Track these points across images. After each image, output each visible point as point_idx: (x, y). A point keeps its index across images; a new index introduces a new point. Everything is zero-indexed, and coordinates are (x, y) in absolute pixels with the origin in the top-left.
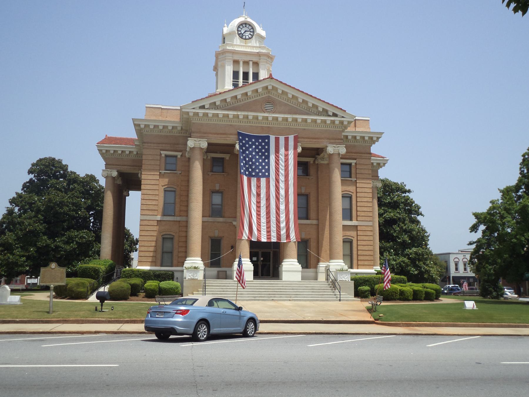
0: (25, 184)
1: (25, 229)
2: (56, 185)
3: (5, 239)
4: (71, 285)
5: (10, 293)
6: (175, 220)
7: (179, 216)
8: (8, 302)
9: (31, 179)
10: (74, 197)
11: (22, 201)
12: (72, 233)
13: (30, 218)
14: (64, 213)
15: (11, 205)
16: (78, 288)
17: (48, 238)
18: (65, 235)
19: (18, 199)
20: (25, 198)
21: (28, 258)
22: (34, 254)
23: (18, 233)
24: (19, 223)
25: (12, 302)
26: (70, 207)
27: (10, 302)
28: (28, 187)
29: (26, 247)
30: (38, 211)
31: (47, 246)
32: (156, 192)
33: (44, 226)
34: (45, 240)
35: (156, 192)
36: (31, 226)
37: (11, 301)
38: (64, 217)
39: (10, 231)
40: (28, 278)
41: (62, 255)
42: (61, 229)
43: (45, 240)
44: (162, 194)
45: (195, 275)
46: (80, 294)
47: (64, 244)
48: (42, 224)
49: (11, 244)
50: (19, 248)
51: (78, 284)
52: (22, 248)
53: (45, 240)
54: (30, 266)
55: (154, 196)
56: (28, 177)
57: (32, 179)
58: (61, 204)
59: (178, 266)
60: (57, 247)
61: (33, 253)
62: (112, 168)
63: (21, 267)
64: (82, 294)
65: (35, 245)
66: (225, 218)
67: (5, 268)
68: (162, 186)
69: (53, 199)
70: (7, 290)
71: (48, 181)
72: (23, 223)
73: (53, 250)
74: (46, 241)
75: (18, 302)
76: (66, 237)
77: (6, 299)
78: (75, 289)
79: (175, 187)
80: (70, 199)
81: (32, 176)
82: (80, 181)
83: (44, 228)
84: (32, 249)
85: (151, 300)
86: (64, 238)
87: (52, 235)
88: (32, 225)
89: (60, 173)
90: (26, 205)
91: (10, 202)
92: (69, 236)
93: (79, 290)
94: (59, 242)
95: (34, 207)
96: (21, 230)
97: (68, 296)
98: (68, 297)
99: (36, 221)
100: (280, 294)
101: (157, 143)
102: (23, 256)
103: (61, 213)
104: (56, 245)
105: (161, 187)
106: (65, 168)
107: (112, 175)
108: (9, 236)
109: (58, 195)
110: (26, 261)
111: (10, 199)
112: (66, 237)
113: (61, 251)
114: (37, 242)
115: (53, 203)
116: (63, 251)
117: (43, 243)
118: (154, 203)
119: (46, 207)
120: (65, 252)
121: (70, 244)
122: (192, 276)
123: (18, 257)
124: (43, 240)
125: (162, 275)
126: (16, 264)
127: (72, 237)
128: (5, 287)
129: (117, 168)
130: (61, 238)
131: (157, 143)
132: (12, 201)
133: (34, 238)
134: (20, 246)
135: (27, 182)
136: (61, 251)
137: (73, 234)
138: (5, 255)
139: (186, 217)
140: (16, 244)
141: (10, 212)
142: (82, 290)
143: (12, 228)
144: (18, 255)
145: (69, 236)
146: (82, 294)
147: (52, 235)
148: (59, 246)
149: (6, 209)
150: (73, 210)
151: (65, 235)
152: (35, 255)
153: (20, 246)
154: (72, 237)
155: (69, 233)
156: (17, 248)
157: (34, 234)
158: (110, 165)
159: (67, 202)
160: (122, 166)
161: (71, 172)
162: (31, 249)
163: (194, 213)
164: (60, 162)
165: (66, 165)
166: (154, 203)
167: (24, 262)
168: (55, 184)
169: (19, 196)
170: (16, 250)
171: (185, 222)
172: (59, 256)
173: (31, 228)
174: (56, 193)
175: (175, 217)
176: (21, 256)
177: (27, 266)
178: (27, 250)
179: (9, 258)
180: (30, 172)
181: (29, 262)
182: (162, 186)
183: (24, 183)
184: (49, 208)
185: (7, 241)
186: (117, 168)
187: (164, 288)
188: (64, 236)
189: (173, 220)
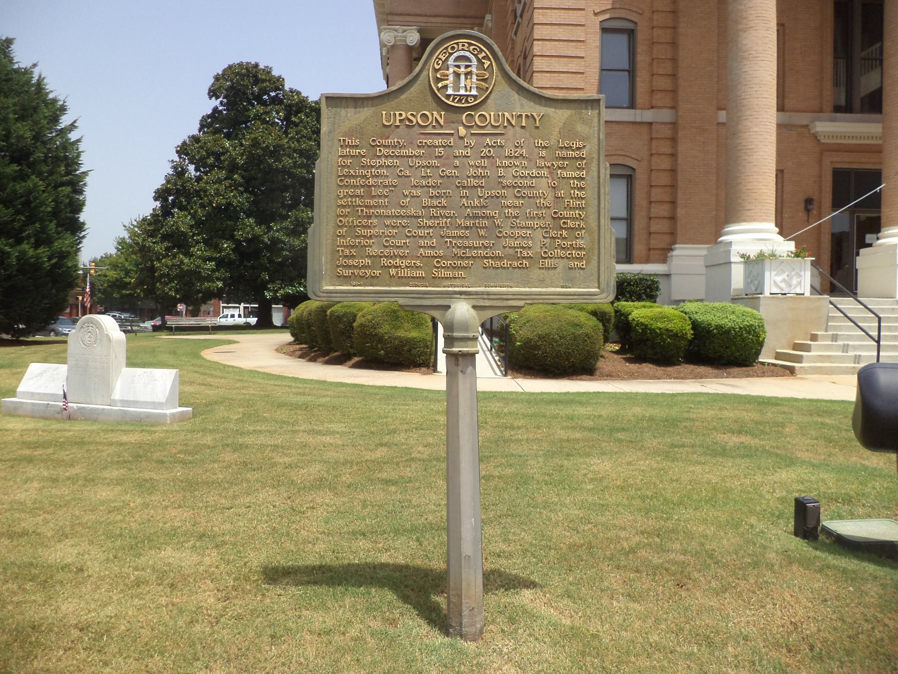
0: (204, 119)
1: (211, 203)
2: (263, 116)
3: (173, 225)
4: (369, 317)
5: (122, 357)
6: (638, 120)
7: (649, 109)
8: (113, 403)
9: (215, 110)
10: (301, 138)
11: (201, 147)
12: (303, 212)
13: (219, 181)
14: (285, 171)
15: (180, 158)
16: (397, 328)
17: (255, 222)
18: (289, 217)
19: (193, 145)
20: (205, 143)
21: (220, 263)
22: (230, 254)
23: (196, 212)
24: (197, 193)
25: (135, 403)
26: (296, 158)
27: (125, 403)
28: (209, 125)
29: (215, 240)
30: (233, 168)
31: (256, 239)
32: (579, 33)
33: (247, 198)
34: (251, 226)
35: (579, 33)
36: (221, 195)
37: (131, 398)
38: (284, 179)
39: (181, 208)
40: (224, 307)
41: (286, 258)
42: (280, 205)
43: (249, 227)
44: (594, 39)
45: (794, 282)
46: (410, 351)
47: (288, 235)
48: (242, 193)
49: (184, 234)
50: (200, 243)
51: (395, 312)
52: (206, 242)
53: (249, 227)
54: (224, 280)
55: (575, 44)
56: (209, 105)
57: (217, 108)
58: (276, 152)
59: (647, 261)
60: (275, 241)
61: (228, 254)
62: (406, 24)
63: (208, 281)
64: (414, 351)
65: (232, 237)
66: (788, 114)
67: (177, 284)
68: (596, 14)
69: (261, 140)
70: (109, 340)
71: (248, 110)
72: (205, 191)
73: (268, 248)
74: (253, 229)
75: (168, 402)
76: (290, 222)
77: (108, 387)
78: (385, 329)
79: (634, 17)
80: (293, 143)
81: (215, 103)
82: (311, 107)
83: (248, 202)
84: (225, 246)
85: (680, 372)
86: (287, 223)
87: (264, 218)
88: (222, 193)
89: (269, 95)
90: (208, 157)
91: (177, 152)
92: (297, 219)
93: (401, 333)
94: (277, 231)
95: (224, 161)
96: (203, 206)
97: (355, 355)
98: (356, 359)
99: (230, 186)
100: (889, 346)
101: (471, 17)
102: (210, 259)
103: (277, 171)
104: (273, 238)
105: (593, 17)
106: (277, 84)
107: (405, 41)
108: (179, 218)
109: (270, 134)
110: (217, 270)
111: (178, 146)
112: (290, 222)
113: (282, 249)
114: (234, 230)
115: (262, 149)
116: (286, 250)
117: (248, 233)
118: (573, 66)
119: (247, 158)
120: (290, 251)
121: (300, 236)
122: (783, 285)
123: (199, 262)
124: (247, 226)
125: (629, 284)
126: (196, 274)
127: (302, 220)
128: (98, 325)
129: (419, 24)
130: (282, 223)
131: (471, 17)
132: (182, 150)
133: (229, 223)
134: (203, 238)
135: (209, 116)
136: (282, 249)
137: (304, 215)
138: (174, 256)
139: (670, 111)
140: (194, 235)
141: (179, 172)
142: (414, 334)
143: (184, 203)
144: (200, 257)
145: (297, 219)
146: (414, 351)
147: (264, 218)
148: (278, 238)
149: (170, 165)
150: (302, 166)
151: (289, 217)
152: (233, 257)
153: (203, 238)
154: (302, 220)
155: (297, 213)
156: (198, 242)
157: (228, 212)
158: (400, 15)
159: (289, 148)
160: (431, 16)
161: (291, 91)
162: (223, 245)
163: (756, 68)
164: (268, 71)
165: (280, 77)
166: (573, 66)
167: (213, 271)
168: (262, 114)
169: (195, 139)
170: (194, 247)
171: (669, 126)
172: (280, 260)
173: (220, 200)
174: (266, 130)
175: (638, 112)
176: (206, 259)
177: (218, 279)
178: (217, 248)
179: (182, 262)
180: (213, 93)
181: (223, 273)
182: (596, 14)
183: (203, 117)
184: (254, 161)
185: (177, 228)
186: (419, 24)
187: (719, 327)
188: (287, 220)
189: (631, 119)
